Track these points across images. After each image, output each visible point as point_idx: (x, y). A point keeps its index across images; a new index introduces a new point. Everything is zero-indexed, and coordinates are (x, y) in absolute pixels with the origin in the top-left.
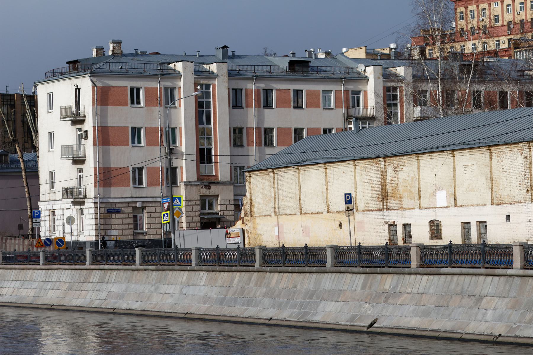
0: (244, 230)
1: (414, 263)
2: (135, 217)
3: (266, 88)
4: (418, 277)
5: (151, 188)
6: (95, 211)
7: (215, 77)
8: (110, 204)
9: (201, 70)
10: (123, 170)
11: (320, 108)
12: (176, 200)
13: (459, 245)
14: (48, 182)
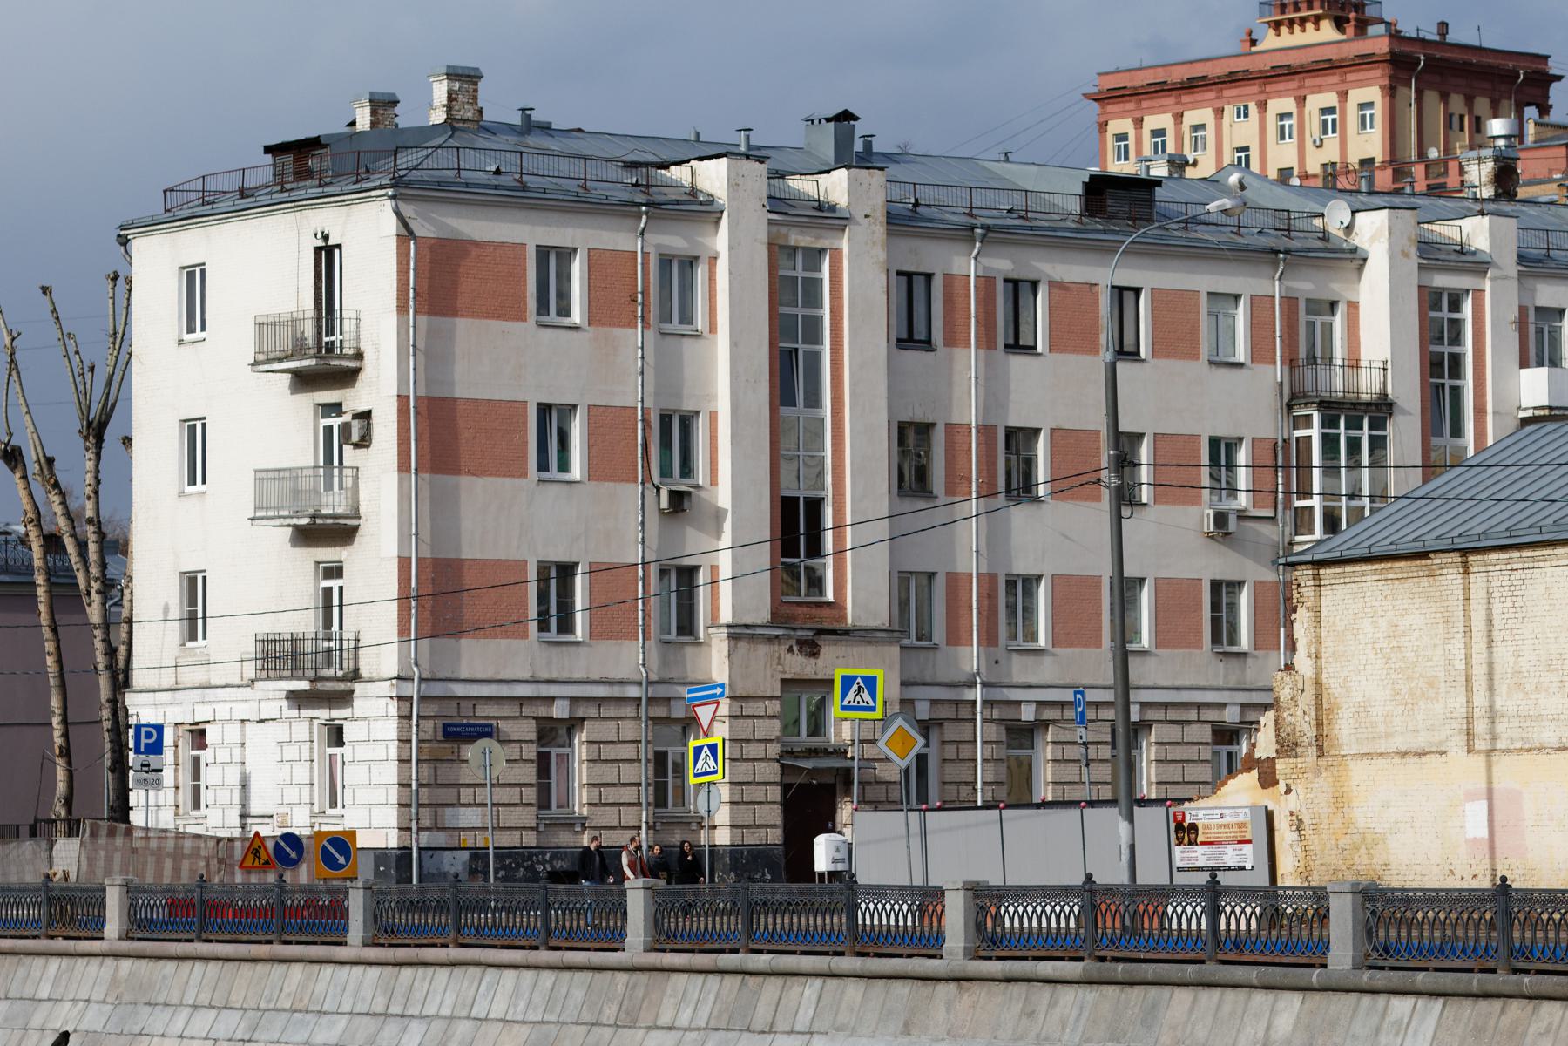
1: (1342, 954)
2: (660, 759)
3: (1015, 276)
5: (605, 647)
8: (454, 704)
9: (778, 196)
10: (505, 575)
11: (1198, 358)
12: (855, 687)
13: (1122, 885)
14: (175, 613)
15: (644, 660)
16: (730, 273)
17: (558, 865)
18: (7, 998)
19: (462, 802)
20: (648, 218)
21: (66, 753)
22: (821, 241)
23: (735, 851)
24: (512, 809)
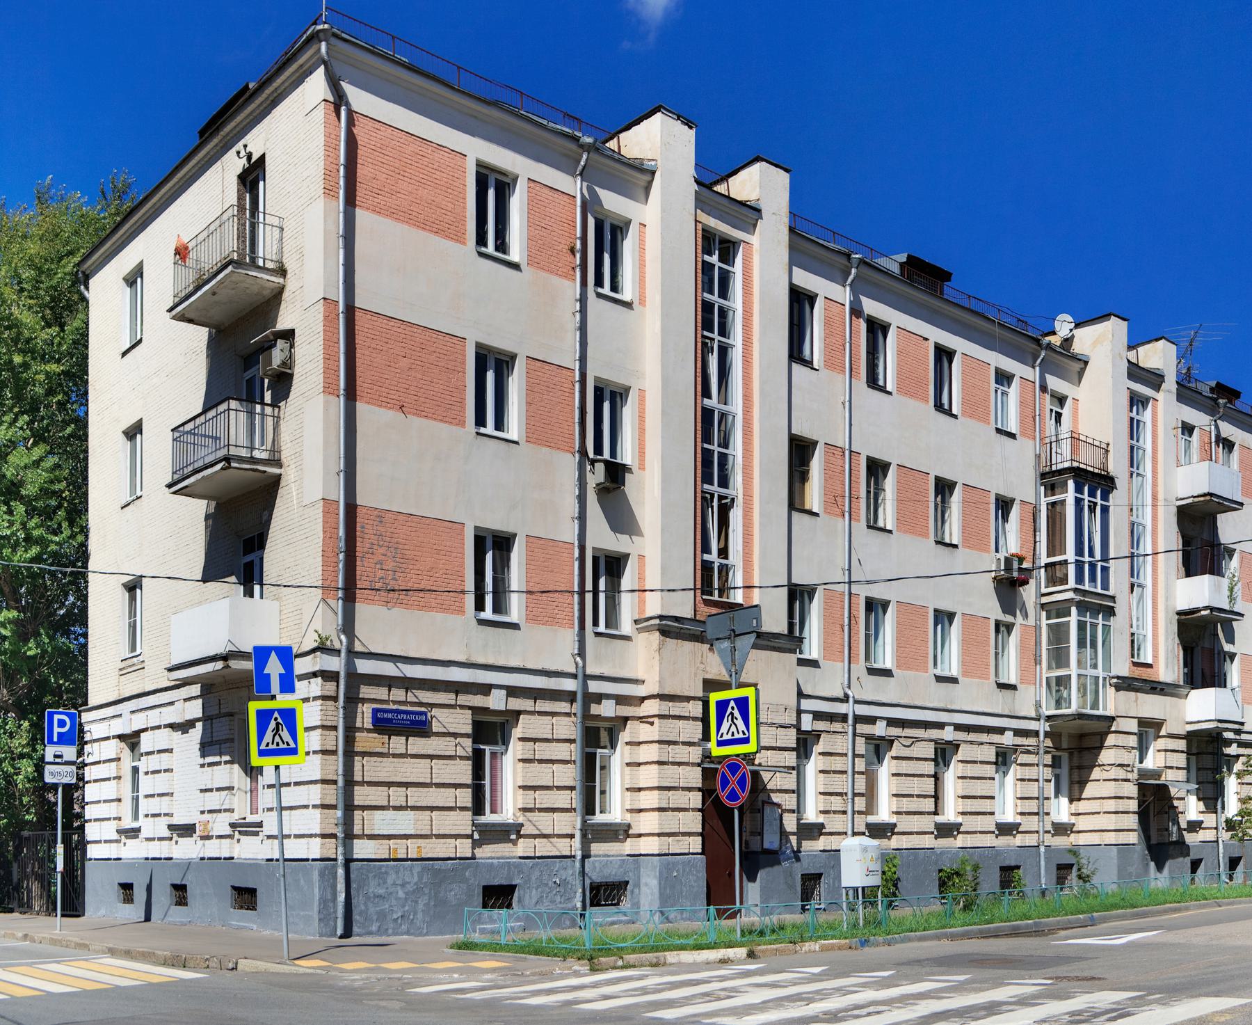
0: (943, 728)
11: (496, 429)
21: (1039, 415)
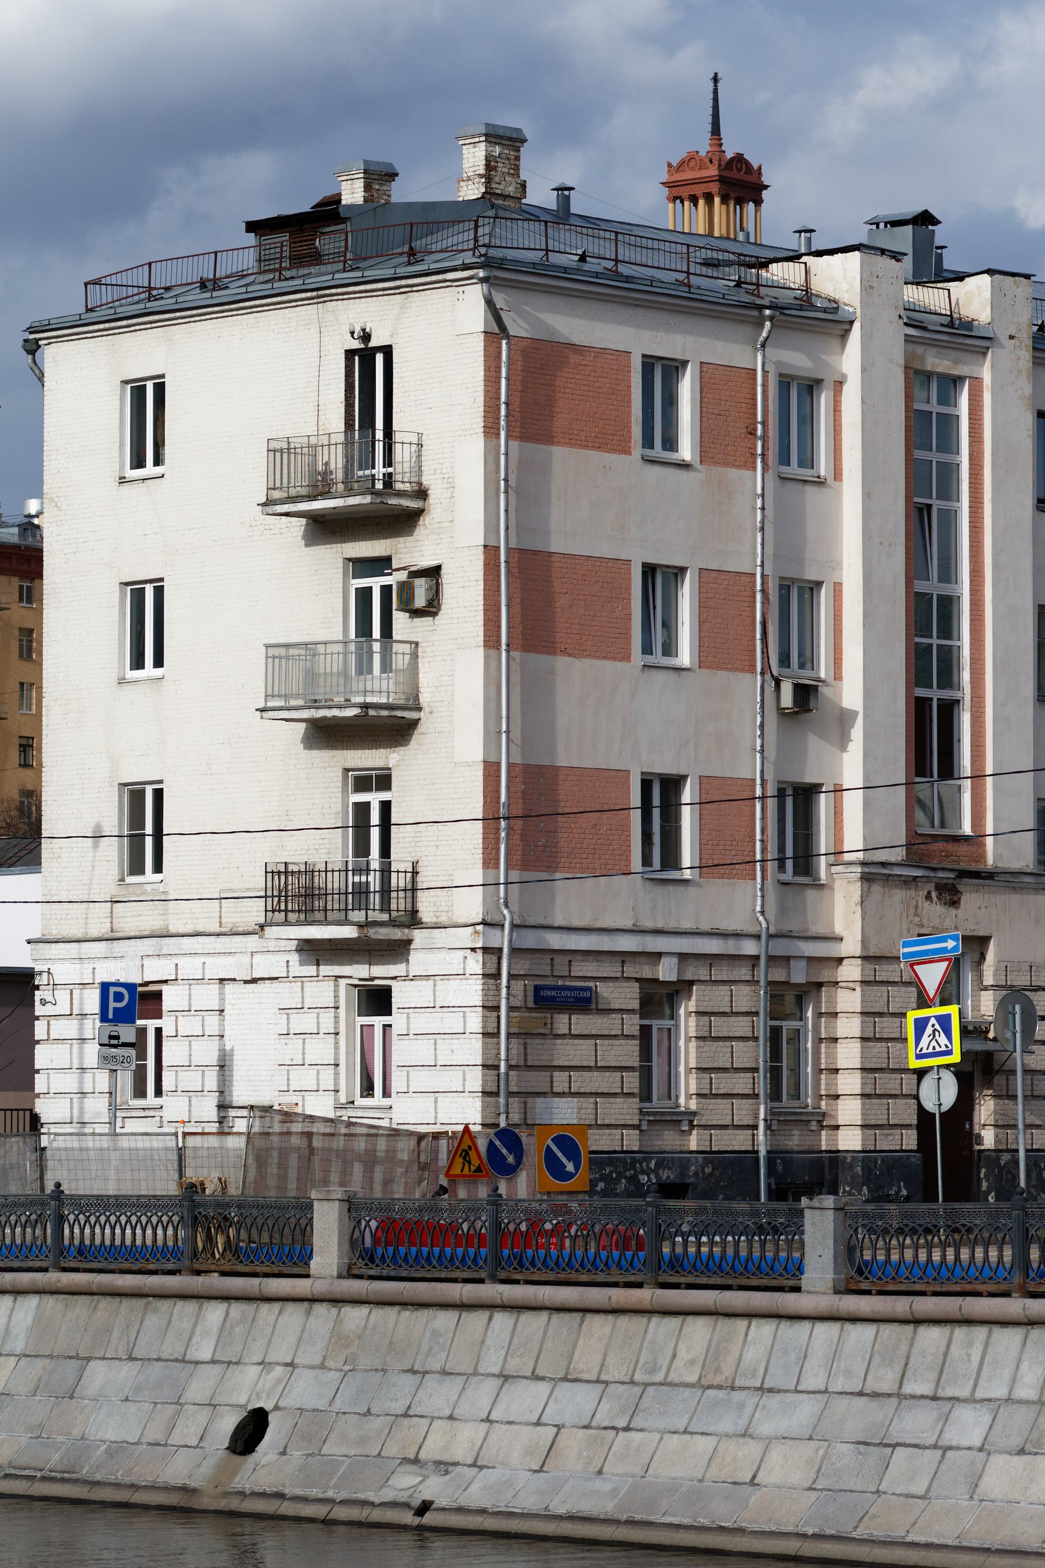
2: (775, 1035)
4: (239, 1098)
5: (716, 888)
6: (485, 991)
7: (985, 343)
8: (547, 959)
15: (763, 906)
16: (863, 402)
17: (665, 1175)
18: (131, 1359)
19: (555, 1090)
20: (772, 326)
22: (960, 366)
23: (868, 1157)
24: (612, 1100)
